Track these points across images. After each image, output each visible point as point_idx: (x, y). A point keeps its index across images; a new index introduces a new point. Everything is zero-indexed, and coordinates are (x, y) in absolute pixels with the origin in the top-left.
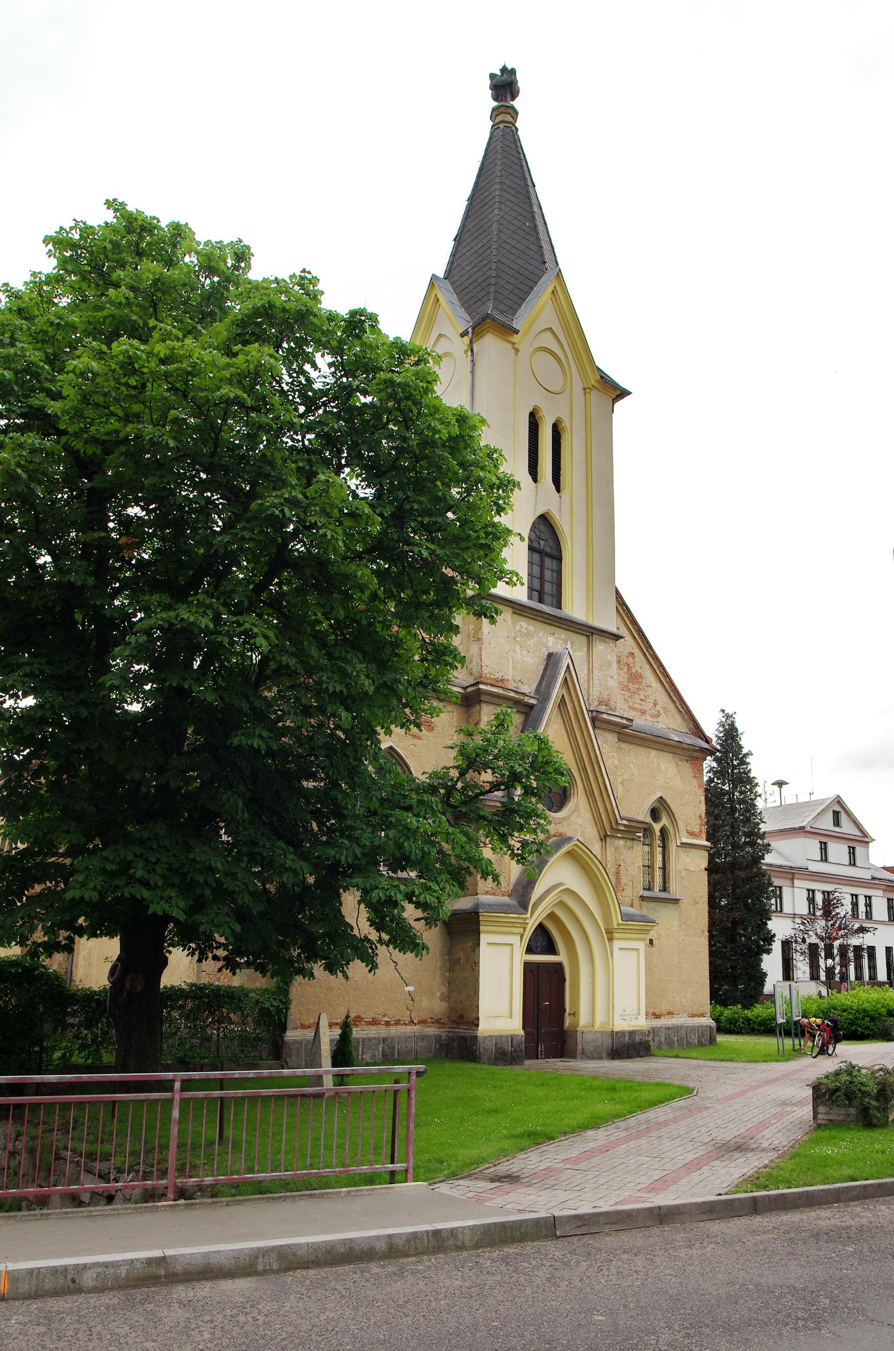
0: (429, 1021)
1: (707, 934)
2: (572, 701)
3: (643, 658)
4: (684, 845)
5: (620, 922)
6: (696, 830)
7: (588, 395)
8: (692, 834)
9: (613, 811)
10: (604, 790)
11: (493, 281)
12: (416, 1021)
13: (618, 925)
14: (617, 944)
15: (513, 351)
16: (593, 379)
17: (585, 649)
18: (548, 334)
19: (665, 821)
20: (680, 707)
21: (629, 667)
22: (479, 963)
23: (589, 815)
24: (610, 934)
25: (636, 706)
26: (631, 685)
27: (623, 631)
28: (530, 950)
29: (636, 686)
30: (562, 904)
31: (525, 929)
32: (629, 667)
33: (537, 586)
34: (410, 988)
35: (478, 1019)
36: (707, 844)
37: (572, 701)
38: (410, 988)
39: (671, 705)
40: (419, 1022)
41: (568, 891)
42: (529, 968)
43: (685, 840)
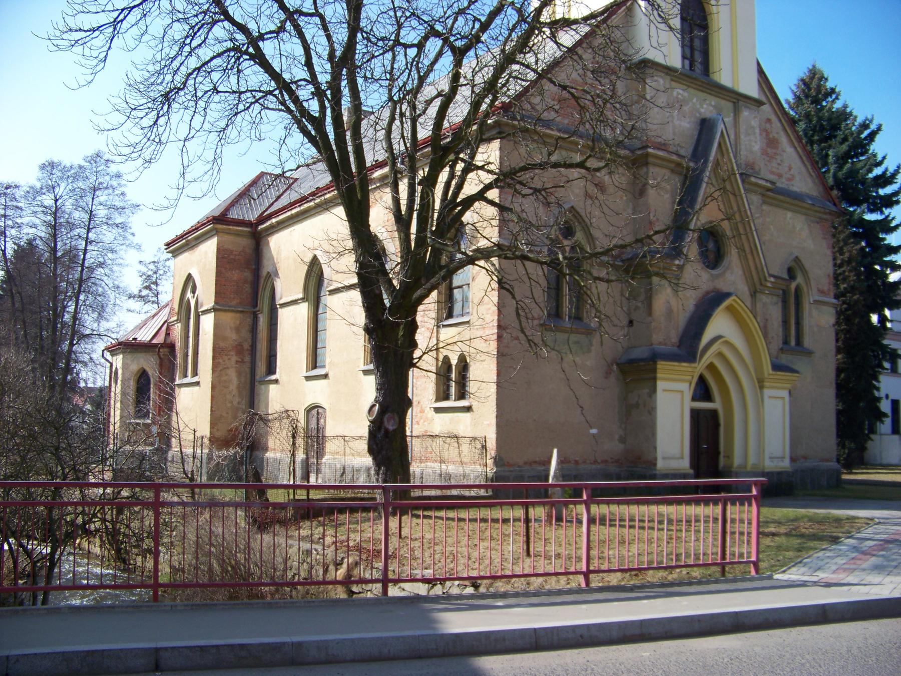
3: (779, 125)
4: (816, 302)
5: (771, 372)
6: (826, 288)
8: (822, 292)
9: (762, 269)
10: (753, 250)
11: (33, 331)
12: (599, 461)
13: (769, 374)
14: (767, 392)
17: (732, 115)
19: (800, 279)
21: (767, 133)
23: (740, 272)
24: (761, 384)
25: (774, 170)
26: (769, 150)
27: (763, 99)
28: (694, 399)
29: (774, 151)
30: (720, 355)
31: (693, 377)
32: (767, 133)
33: (688, 55)
34: (594, 431)
35: (656, 459)
38: (594, 431)
40: (602, 462)
41: (727, 343)
43: (817, 298)
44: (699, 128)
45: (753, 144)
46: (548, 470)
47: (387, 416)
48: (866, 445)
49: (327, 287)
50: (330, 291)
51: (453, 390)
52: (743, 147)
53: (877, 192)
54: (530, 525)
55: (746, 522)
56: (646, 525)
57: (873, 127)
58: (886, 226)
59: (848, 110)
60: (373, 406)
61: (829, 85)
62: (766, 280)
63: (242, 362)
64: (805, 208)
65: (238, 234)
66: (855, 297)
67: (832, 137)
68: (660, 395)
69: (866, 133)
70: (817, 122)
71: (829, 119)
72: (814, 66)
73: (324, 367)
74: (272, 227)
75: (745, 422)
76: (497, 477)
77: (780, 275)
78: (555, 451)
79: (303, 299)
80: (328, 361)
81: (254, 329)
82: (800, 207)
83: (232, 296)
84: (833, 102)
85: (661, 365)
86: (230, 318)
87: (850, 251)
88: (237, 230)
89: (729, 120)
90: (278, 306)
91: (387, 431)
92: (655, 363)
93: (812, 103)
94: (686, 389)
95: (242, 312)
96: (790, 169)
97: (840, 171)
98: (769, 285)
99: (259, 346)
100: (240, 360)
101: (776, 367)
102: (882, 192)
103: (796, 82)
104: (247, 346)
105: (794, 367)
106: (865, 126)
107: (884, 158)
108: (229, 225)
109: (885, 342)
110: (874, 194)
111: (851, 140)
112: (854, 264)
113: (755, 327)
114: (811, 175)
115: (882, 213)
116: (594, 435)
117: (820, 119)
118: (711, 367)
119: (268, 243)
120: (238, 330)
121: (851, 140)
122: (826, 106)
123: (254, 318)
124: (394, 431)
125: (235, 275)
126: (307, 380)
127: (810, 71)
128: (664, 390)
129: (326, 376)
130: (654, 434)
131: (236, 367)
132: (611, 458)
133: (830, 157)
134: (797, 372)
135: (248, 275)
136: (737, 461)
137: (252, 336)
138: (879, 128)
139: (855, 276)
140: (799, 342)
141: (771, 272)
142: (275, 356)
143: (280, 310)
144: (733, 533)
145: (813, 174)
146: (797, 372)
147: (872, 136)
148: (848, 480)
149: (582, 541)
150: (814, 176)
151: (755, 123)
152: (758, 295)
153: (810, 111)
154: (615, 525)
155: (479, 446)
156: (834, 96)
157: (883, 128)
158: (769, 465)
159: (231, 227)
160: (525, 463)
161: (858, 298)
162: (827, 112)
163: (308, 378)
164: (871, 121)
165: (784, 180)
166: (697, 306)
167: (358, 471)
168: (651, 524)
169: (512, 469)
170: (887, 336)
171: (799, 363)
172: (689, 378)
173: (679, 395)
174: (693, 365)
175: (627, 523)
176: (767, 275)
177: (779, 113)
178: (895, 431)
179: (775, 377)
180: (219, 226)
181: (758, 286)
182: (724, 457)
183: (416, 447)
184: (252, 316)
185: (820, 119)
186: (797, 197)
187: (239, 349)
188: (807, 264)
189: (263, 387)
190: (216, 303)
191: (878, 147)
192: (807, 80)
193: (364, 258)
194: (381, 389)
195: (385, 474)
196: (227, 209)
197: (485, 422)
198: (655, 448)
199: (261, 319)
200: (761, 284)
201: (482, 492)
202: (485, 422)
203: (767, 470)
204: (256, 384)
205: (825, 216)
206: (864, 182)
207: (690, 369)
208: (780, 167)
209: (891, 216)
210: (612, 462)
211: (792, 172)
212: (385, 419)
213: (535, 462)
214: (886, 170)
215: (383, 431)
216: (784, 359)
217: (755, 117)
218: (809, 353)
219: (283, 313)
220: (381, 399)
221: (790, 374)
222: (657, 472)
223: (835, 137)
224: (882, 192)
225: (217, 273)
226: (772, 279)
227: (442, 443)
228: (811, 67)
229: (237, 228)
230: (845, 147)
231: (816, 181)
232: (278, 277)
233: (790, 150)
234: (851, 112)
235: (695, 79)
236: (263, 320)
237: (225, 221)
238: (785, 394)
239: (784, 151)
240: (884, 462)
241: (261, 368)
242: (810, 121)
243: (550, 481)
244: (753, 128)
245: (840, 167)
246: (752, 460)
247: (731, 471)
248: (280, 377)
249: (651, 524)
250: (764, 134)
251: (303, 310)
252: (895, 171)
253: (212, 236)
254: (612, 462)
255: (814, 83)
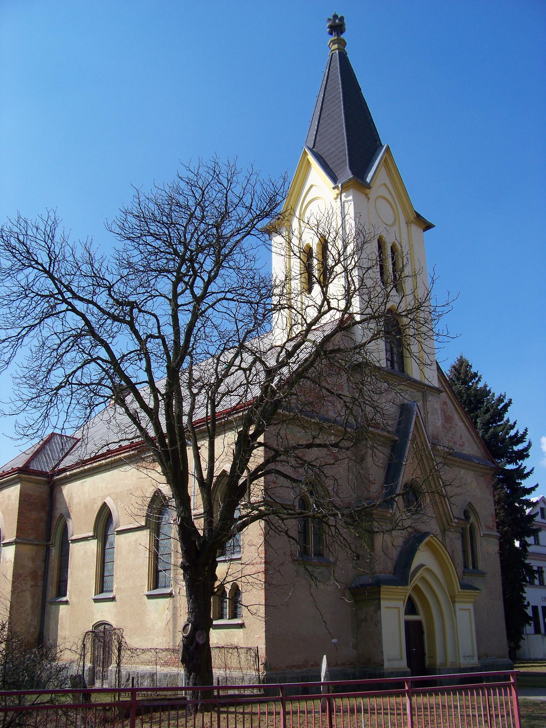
0: (347, 663)
1: (502, 598)
2: (420, 438)
3: (452, 406)
5: (460, 590)
6: (491, 525)
7: (409, 227)
8: (488, 527)
9: (449, 513)
12: (339, 664)
14: (458, 606)
15: (366, 199)
16: (412, 216)
18: (384, 187)
20: (475, 438)
22: (380, 621)
24: (453, 599)
29: (450, 425)
30: (423, 579)
34: (335, 641)
35: (383, 661)
36: (498, 534)
37: (420, 438)
38: (335, 641)
39: (470, 437)
42: (407, 623)
43: (486, 532)
44: (400, 411)
45: (437, 421)
46: (320, 672)
47: (198, 633)
48: (520, 644)
49: (115, 528)
50: (117, 531)
51: (227, 611)
52: (430, 424)
53: (512, 449)
54: (333, 716)
55: (470, 707)
56: (395, 712)
57: (506, 401)
58: (521, 474)
59: (488, 389)
60: (187, 625)
61: (473, 370)
62: (452, 521)
63: (36, 585)
64: (473, 466)
65: (37, 482)
66: (505, 529)
67: (476, 408)
68: (384, 612)
69: (502, 405)
70: (467, 397)
71: (475, 396)
72: (461, 357)
73: (112, 591)
74: (66, 477)
75: (443, 629)
76: (267, 679)
77: (459, 516)
78: (325, 657)
79: (93, 537)
80: (115, 586)
81: (46, 559)
82: (470, 465)
83: (30, 532)
84: (477, 382)
85: (384, 589)
86: (27, 549)
87: (499, 494)
88: (36, 479)
89: (420, 404)
90: (70, 542)
91: (198, 644)
92: (379, 587)
93: (462, 384)
94: (402, 605)
95: (37, 545)
96: (461, 438)
97: (486, 434)
98: (454, 525)
99: (50, 574)
100: (34, 584)
101: (464, 586)
102: (516, 448)
103: (450, 369)
104: (40, 572)
105: (476, 586)
106: (500, 400)
107: (515, 423)
108: (31, 475)
109: (527, 561)
110: (511, 450)
111: (492, 411)
112: (502, 504)
113: (447, 556)
114: (476, 442)
115: (517, 464)
116: (334, 643)
117: (469, 395)
118: (416, 589)
119: (61, 491)
120: (33, 559)
121: (492, 411)
122: (472, 386)
123: (47, 550)
124: (203, 644)
125: (34, 515)
126: (95, 602)
127: (459, 360)
128: (386, 607)
129: (113, 599)
130: (380, 641)
131: (31, 590)
132: (348, 661)
133: (479, 424)
134: (478, 589)
135: (43, 515)
136: (439, 660)
137: (45, 564)
138: (510, 402)
139: (504, 512)
140: (474, 566)
141: (456, 516)
142: (66, 581)
143: (71, 544)
144: (497, 716)
145: (477, 440)
146: (478, 589)
147: (505, 408)
148: (523, 673)
149: (499, 720)
150: (478, 442)
151: (437, 406)
152: (446, 532)
153: (461, 390)
154: (374, 713)
155: (253, 655)
156: (477, 379)
157: (513, 402)
158: (464, 662)
159: (32, 477)
160: (287, 667)
161: (507, 529)
162: (474, 390)
163: (96, 601)
164: (504, 397)
165: (457, 446)
166: (405, 543)
167: (143, 676)
168: (398, 712)
169: (277, 672)
170: (529, 557)
171: (477, 582)
172: (404, 597)
173: (396, 610)
174: (406, 587)
175: (395, 712)
176: (452, 518)
177: (452, 397)
178: (537, 631)
179: (464, 594)
180: (24, 476)
181: (446, 526)
182: (428, 657)
183: (216, 658)
184: (45, 548)
185: (469, 395)
186: (467, 458)
187: (34, 575)
188: (477, 509)
189: (53, 607)
190: (17, 537)
191: (510, 416)
192: (457, 367)
193: (185, 513)
194: (193, 612)
195: (195, 678)
196: (29, 462)
197: (255, 636)
198: (382, 652)
199: (53, 551)
200: (448, 524)
201: (256, 691)
202: (255, 636)
203: (462, 667)
204: (47, 604)
205: (487, 471)
206: (503, 440)
207: (404, 591)
208: (454, 437)
209: (523, 466)
210: (349, 665)
211: (462, 440)
212: (197, 636)
213: (294, 666)
214: (518, 432)
215: (194, 645)
216: (468, 579)
217: (437, 402)
218: (483, 574)
219: (74, 548)
220: (193, 620)
221: (473, 591)
222: (385, 671)
223: (480, 408)
224: (516, 448)
225: (19, 513)
226: (456, 520)
227: (226, 652)
228: (459, 358)
229: (37, 478)
230: (488, 416)
231: (479, 446)
232: (70, 518)
233: (460, 424)
234: (490, 390)
235: (396, 375)
236: (54, 552)
237: (27, 472)
238: (470, 606)
239: (456, 425)
240: (532, 657)
241: (52, 590)
242: (462, 397)
243: (322, 681)
244: (436, 409)
245: (486, 431)
246: (450, 659)
247: (435, 669)
248: (70, 599)
249: (398, 712)
250: (443, 413)
251: (93, 545)
252: (524, 433)
253: (16, 483)
254: (349, 665)
255: (462, 370)
